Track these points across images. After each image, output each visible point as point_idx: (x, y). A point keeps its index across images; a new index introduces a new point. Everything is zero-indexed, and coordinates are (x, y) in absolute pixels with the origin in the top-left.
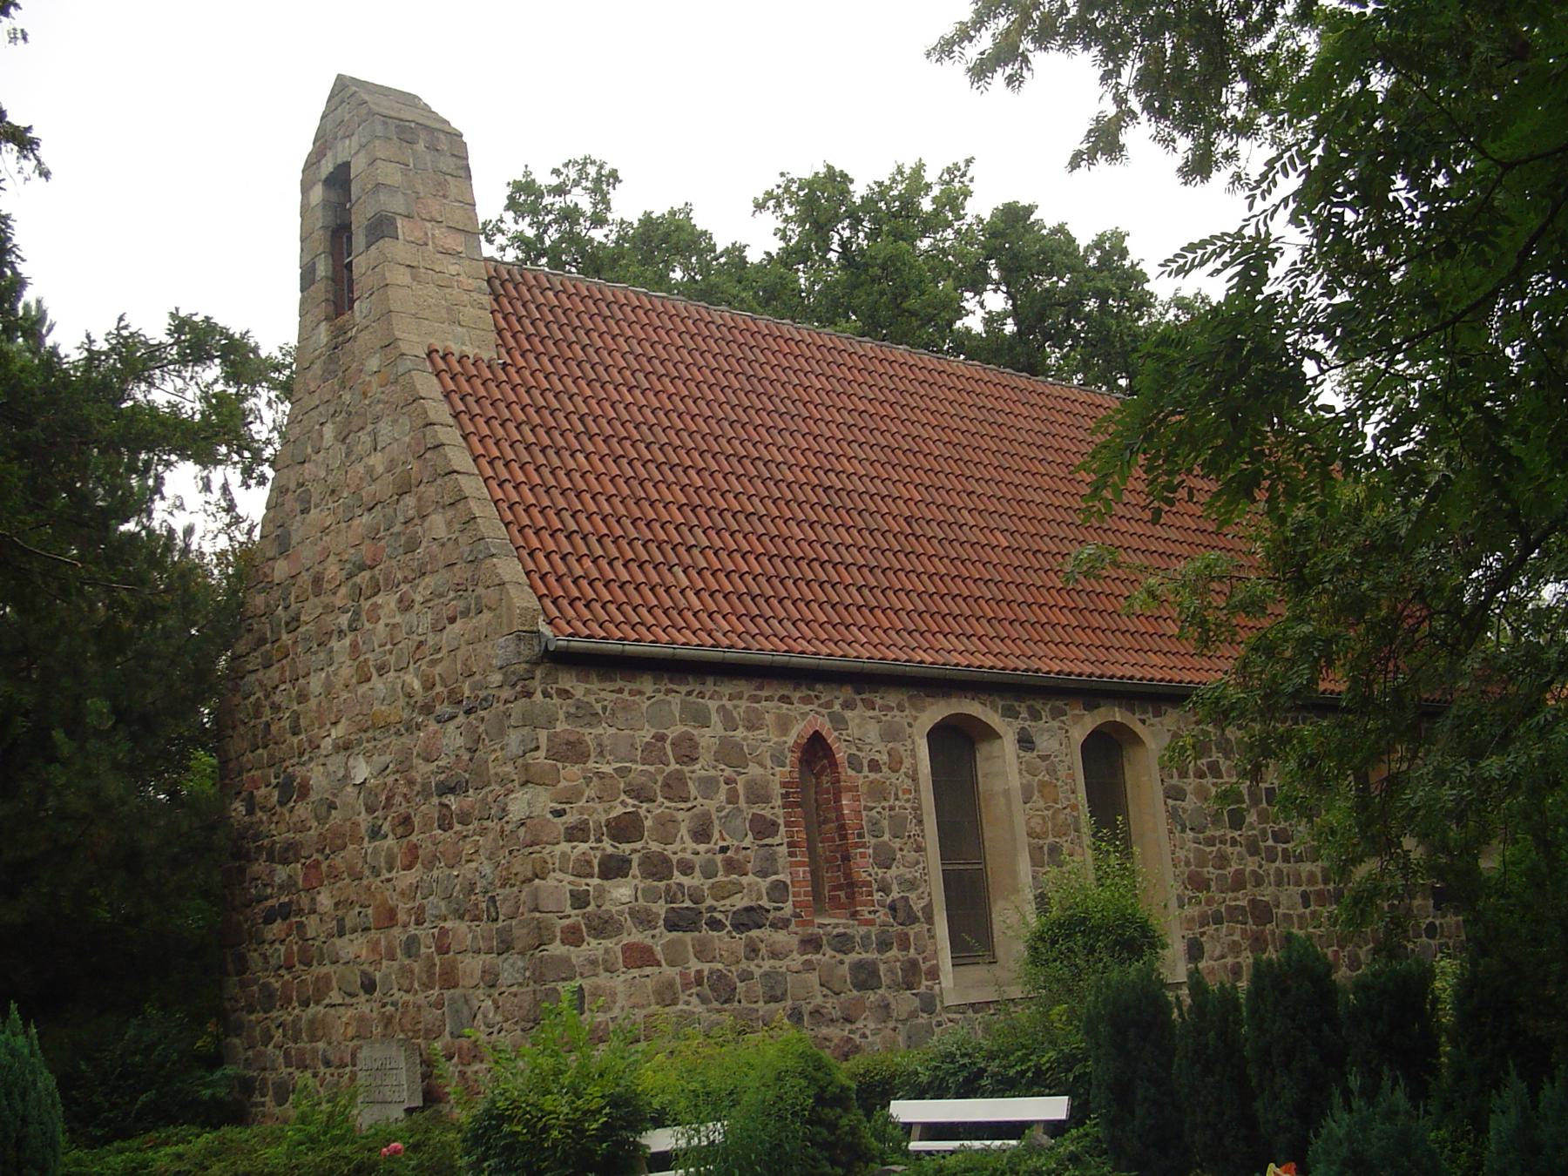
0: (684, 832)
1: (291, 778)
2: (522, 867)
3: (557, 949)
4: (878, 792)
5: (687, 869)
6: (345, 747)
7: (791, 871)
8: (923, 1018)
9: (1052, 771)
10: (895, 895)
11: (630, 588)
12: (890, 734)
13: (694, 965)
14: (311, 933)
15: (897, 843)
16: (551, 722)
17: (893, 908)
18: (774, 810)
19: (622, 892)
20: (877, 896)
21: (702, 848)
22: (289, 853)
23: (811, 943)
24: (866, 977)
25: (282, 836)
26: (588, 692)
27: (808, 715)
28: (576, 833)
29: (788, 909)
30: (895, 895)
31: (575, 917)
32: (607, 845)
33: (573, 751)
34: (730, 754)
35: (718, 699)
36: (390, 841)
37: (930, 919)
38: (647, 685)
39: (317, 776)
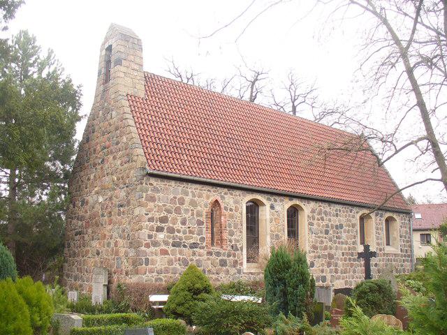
0: (179, 222)
1: (84, 199)
2: (137, 227)
3: (143, 248)
4: (232, 217)
5: (179, 231)
6: (97, 193)
7: (207, 235)
8: (237, 275)
9: (278, 215)
10: (233, 243)
11: (171, 159)
12: (236, 202)
13: (178, 256)
14: (85, 239)
15: (235, 230)
16: (147, 191)
17: (232, 247)
18: (203, 219)
19: (161, 236)
20: (228, 243)
21: (183, 226)
22: (81, 218)
23: (210, 253)
24: (223, 263)
25: (81, 213)
26: (157, 184)
27: (214, 195)
28: (151, 220)
29: (204, 244)
30: (233, 243)
31: (149, 241)
32: (158, 223)
33: (152, 199)
34: (193, 203)
35: (192, 188)
36: (106, 218)
37: (242, 250)
38: (173, 183)
39: (90, 199)
